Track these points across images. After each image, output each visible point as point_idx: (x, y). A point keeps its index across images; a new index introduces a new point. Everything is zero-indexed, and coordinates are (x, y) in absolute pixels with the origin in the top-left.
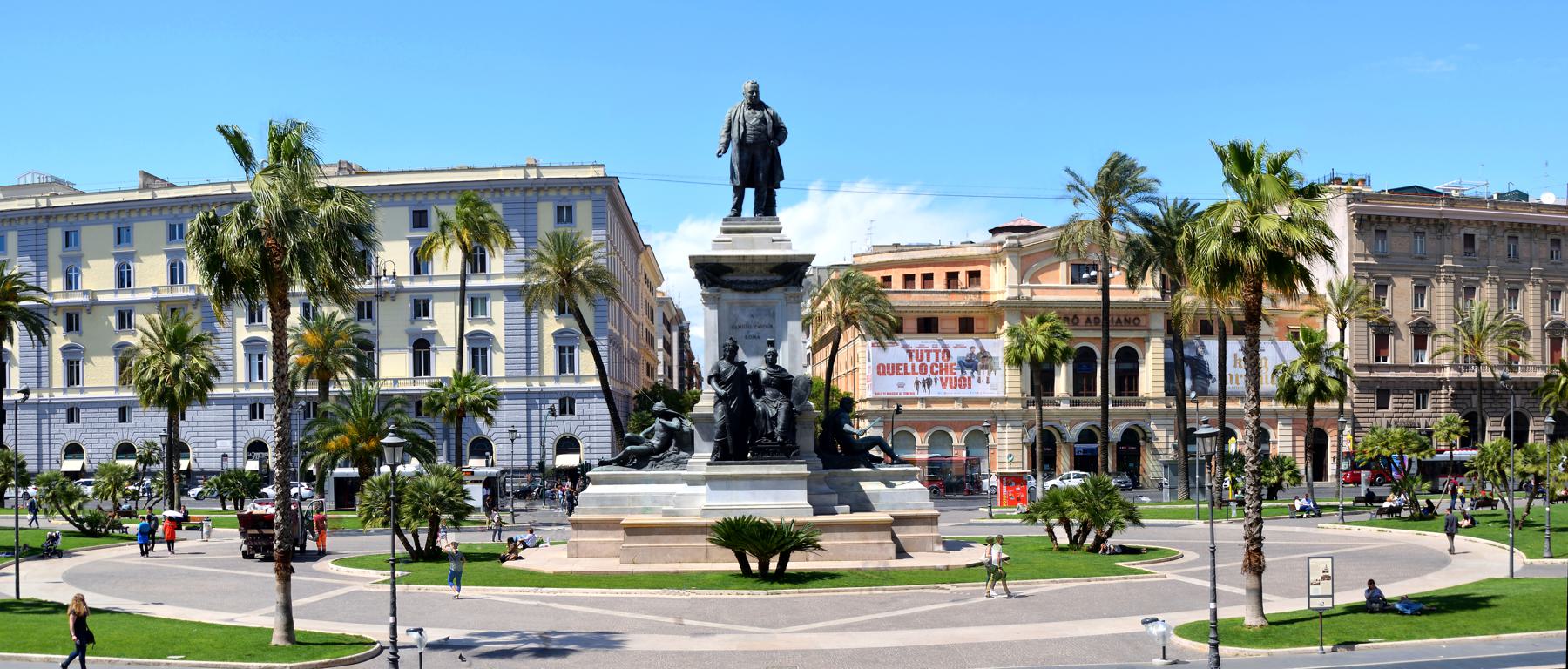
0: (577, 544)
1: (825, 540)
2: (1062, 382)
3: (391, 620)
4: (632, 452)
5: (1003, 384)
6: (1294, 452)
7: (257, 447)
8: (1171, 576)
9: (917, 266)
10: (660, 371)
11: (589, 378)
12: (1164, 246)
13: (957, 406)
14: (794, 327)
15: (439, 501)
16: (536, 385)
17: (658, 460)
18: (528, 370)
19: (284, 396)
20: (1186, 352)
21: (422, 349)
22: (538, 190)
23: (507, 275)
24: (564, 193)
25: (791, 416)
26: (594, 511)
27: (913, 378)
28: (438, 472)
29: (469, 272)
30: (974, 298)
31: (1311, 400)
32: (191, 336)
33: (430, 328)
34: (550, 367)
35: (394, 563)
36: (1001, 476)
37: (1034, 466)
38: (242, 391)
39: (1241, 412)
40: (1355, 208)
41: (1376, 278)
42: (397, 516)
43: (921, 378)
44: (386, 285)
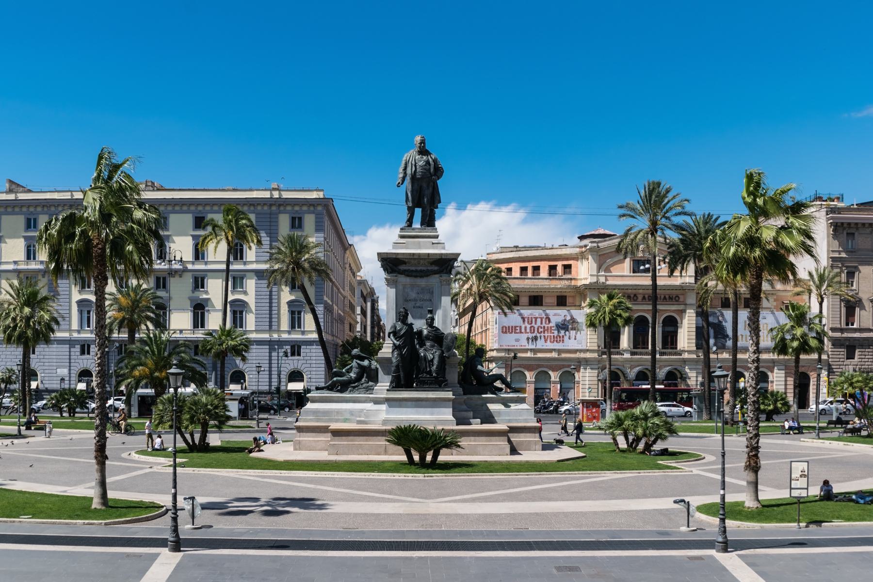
0: (300, 442)
1: (464, 442)
2: (625, 341)
3: (173, 491)
4: (337, 381)
5: (586, 340)
6: (786, 389)
7: (85, 374)
8: (695, 471)
9: (529, 261)
10: (358, 329)
11: (311, 332)
12: (690, 247)
13: (554, 355)
14: (446, 300)
15: (207, 412)
16: (275, 336)
17: (354, 387)
18: (270, 326)
19: (104, 341)
20: (711, 319)
21: (199, 310)
22: (280, 205)
23: (257, 262)
24: (297, 208)
25: (443, 360)
26: (311, 420)
27: (525, 336)
28: (208, 393)
29: (231, 259)
30: (567, 283)
31: (798, 351)
32: (39, 297)
33: (205, 296)
34: (285, 324)
35: (176, 453)
36: (583, 402)
37: (605, 395)
38: (75, 335)
39: (746, 361)
40: (832, 218)
41: (847, 267)
42: (179, 420)
43: (530, 335)
44: (176, 266)
